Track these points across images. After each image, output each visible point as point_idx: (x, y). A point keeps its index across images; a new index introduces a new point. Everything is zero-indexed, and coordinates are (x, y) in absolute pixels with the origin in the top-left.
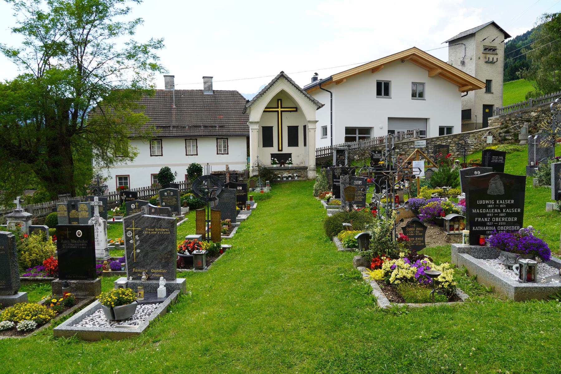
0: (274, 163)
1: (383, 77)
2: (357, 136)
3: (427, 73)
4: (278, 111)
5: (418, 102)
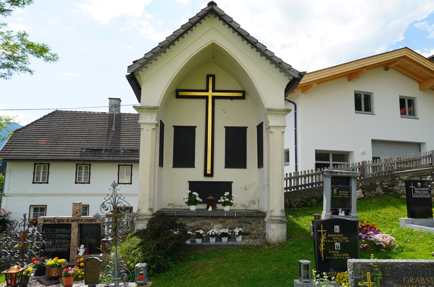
0: (192, 201)
1: (363, 86)
2: (331, 162)
3: (417, 85)
4: (206, 98)
5: (408, 121)
